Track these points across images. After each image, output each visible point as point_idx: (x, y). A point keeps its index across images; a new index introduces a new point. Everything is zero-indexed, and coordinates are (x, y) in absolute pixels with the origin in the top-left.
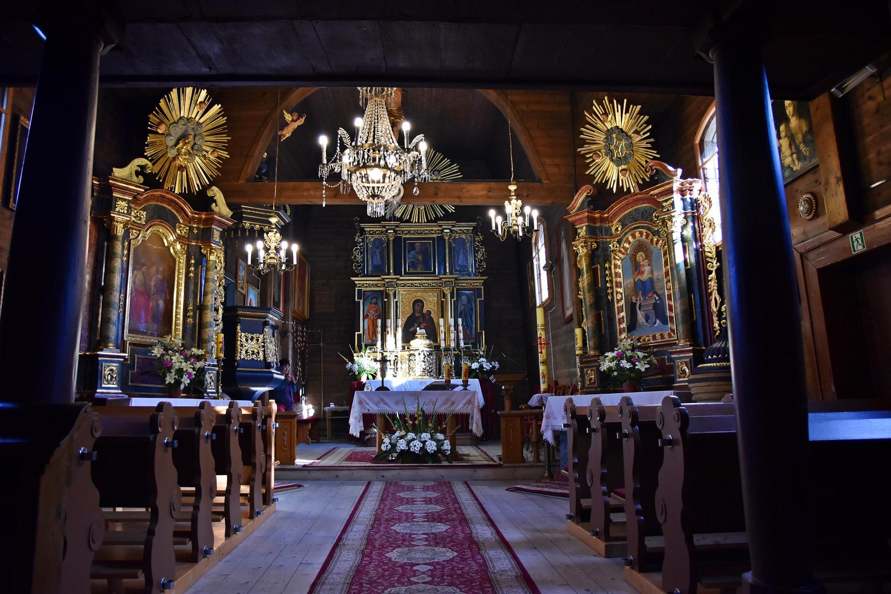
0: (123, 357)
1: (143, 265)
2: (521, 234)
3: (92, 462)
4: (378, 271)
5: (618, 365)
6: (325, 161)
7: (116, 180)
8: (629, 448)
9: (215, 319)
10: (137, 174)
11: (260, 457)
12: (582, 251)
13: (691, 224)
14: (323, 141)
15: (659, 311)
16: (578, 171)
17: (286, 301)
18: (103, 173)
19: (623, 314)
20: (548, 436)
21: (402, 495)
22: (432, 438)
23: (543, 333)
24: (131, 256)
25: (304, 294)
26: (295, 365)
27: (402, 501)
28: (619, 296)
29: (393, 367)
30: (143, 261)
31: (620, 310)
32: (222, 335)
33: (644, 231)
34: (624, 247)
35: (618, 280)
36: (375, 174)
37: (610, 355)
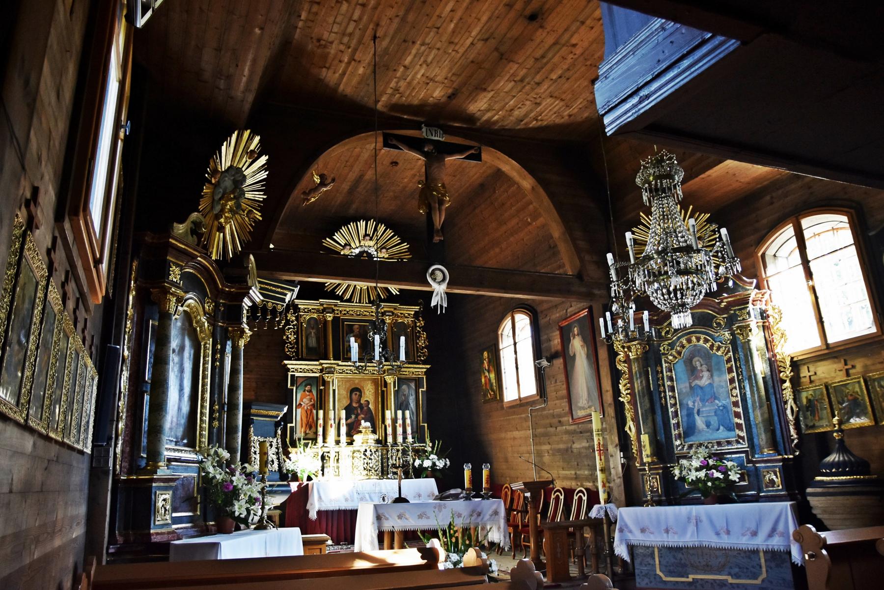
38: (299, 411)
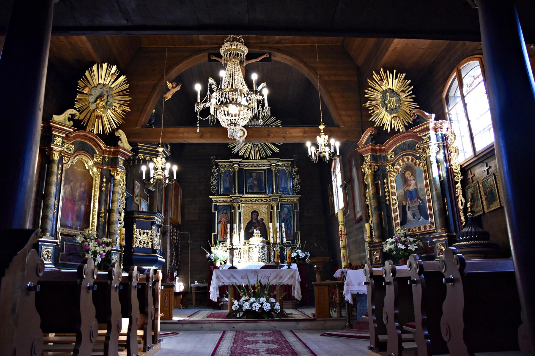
0: (56, 243)
1: (71, 181)
2: (328, 159)
3: (37, 293)
4: (228, 192)
5: (396, 247)
6: (199, 101)
7: (55, 123)
8: (417, 291)
9: (119, 218)
10: (69, 119)
11: (151, 309)
12: (368, 172)
13: (442, 151)
14: (198, 87)
15: (422, 211)
16: (364, 118)
17: (166, 211)
18: (47, 119)
19: (397, 213)
20: (348, 298)
21: (248, 338)
22: (267, 301)
23: (343, 227)
24: (63, 175)
25: (177, 207)
26: (171, 255)
27: (248, 342)
28: (394, 201)
29: (238, 256)
30: (71, 178)
31: (395, 211)
32: (124, 229)
33: (410, 157)
34: (396, 169)
35: (393, 190)
36: (233, 109)
37: (390, 240)
38: (220, 225)
